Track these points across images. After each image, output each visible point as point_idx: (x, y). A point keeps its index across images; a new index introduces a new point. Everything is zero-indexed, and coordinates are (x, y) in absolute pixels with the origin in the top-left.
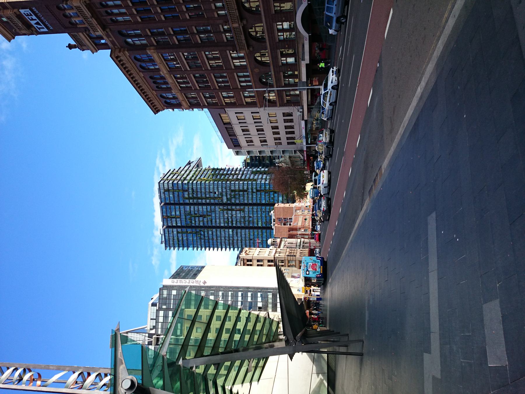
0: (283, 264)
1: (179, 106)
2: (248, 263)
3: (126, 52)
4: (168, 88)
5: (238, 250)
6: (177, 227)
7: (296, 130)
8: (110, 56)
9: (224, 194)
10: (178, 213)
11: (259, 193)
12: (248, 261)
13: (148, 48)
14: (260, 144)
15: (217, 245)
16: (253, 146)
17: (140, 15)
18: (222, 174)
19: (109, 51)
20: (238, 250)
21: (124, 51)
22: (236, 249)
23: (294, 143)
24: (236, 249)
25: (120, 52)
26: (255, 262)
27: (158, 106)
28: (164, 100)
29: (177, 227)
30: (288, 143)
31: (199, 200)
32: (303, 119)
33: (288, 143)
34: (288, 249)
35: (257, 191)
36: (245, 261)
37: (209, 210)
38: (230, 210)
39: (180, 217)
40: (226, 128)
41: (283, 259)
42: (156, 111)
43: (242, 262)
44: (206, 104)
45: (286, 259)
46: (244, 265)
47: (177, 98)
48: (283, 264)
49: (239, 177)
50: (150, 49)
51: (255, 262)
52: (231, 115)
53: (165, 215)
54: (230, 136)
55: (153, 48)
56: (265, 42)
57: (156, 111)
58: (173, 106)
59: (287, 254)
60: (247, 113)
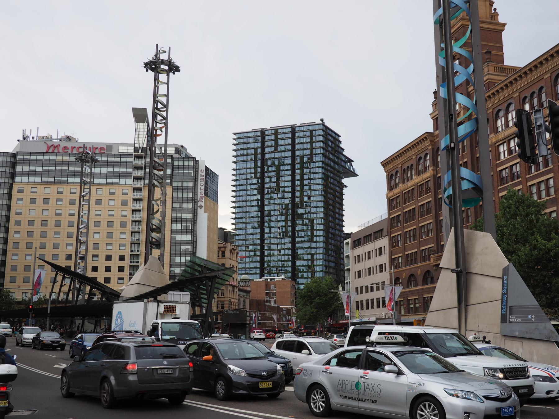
0: (220, 296)
1: (390, 188)
2: (221, 253)
3: (431, 147)
4: (404, 180)
5: (232, 230)
6: (263, 147)
7: (371, 312)
8: (427, 133)
9: (308, 210)
10: (282, 148)
11: (309, 257)
12: (223, 253)
13: (435, 168)
14: (357, 270)
15: (239, 201)
16: (354, 262)
17: (402, 214)
18: (334, 207)
19: (432, 130)
20: (232, 230)
21: (432, 145)
22: (234, 227)
23: (357, 308)
24: (234, 227)
25: (431, 141)
26: (369, 401)
27: (391, 166)
28: (394, 174)
29: (263, 147)
30: (357, 302)
31: (299, 187)
32: (377, 319)
33: (357, 302)
34: (237, 301)
35: (312, 255)
36: (222, 249)
37: (287, 189)
38: (286, 218)
39: (276, 150)
40: (371, 234)
41: (225, 295)
42: (385, 164)
43: (222, 245)
44: (391, 217)
45: (226, 299)
46: (219, 248)
47: (396, 187)
48: (220, 296)
49: (331, 230)
50: (433, 170)
51: (369, 401)
52: (384, 242)
53: (279, 131)
54: (364, 237)
55: (435, 172)
56: (423, 285)
57: (385, 164)
58: (390, 178)
59: (232, 300)
60: (385, 259)
